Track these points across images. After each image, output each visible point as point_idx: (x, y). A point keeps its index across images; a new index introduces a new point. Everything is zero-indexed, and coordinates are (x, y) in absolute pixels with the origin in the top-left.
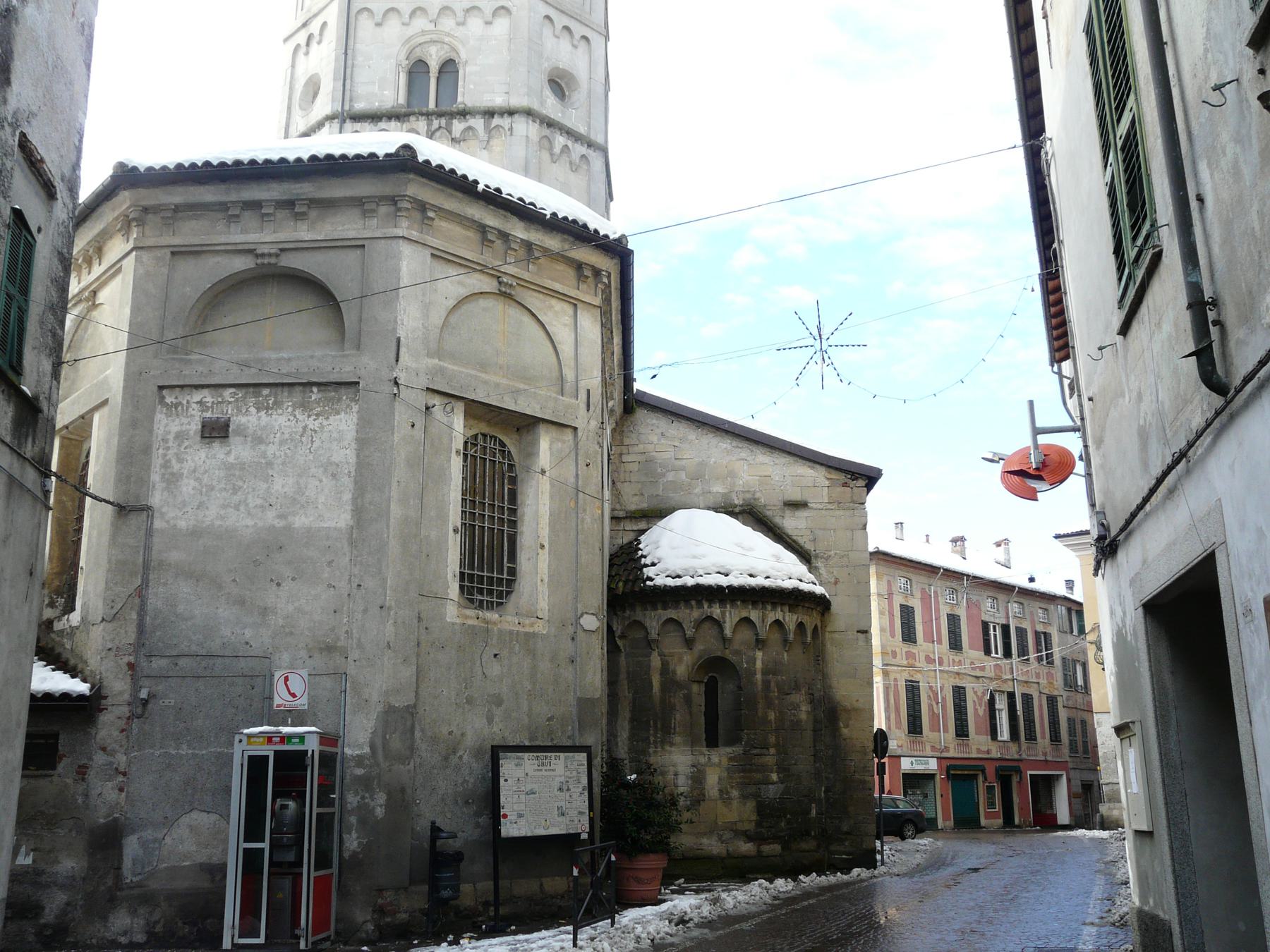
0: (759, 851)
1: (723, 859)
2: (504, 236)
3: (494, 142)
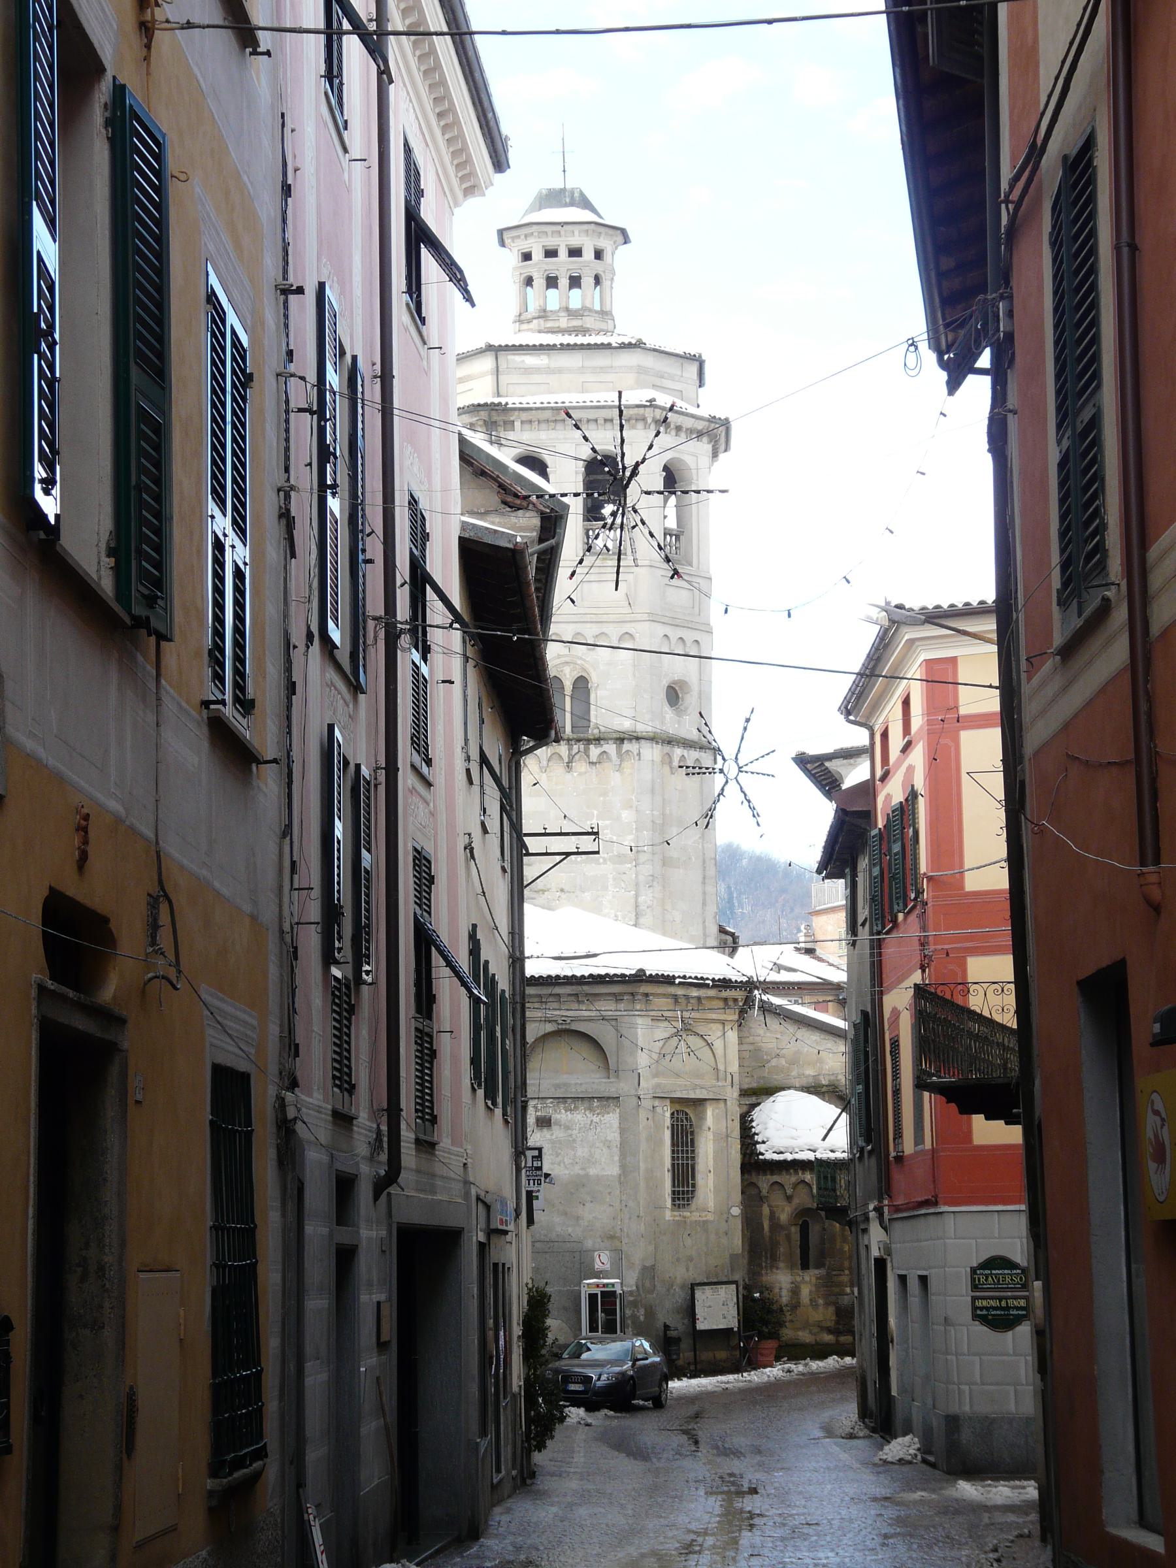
0: (837, 1341)
1: (812, 1345)
2: (687, 997)
3: (625, 764)
